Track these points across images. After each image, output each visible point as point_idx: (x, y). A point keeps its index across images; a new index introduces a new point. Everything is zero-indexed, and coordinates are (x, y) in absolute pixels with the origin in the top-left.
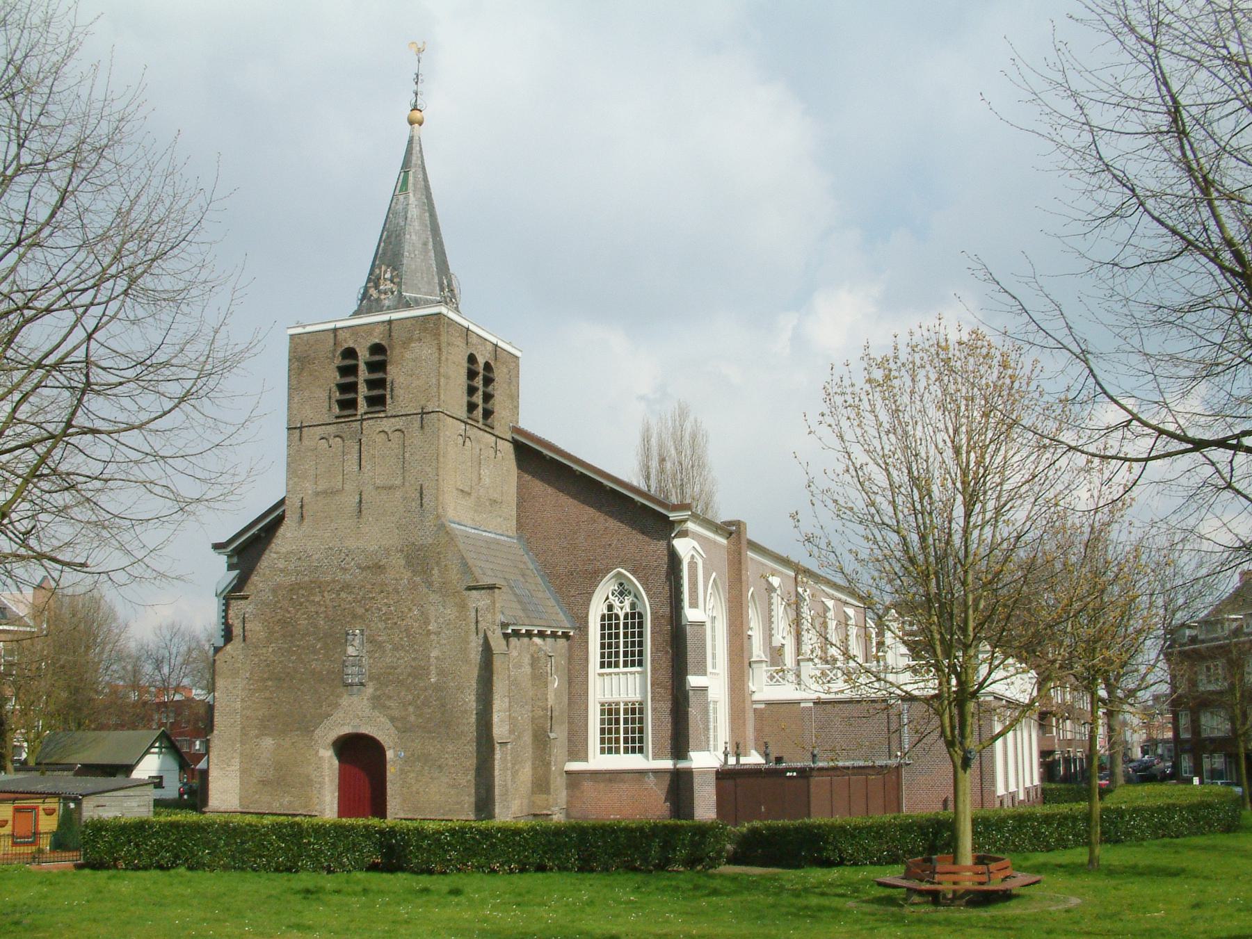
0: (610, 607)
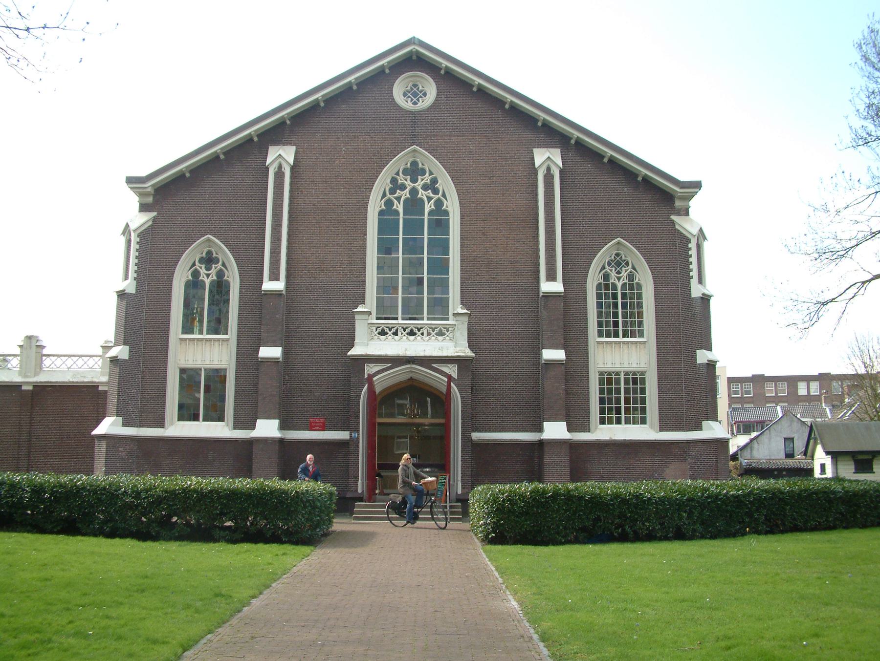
0: (606, 277)
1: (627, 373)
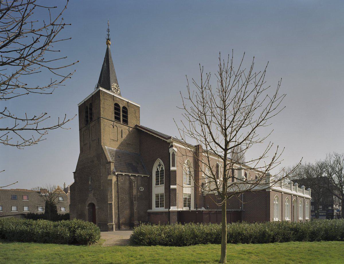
0: (157, 169)
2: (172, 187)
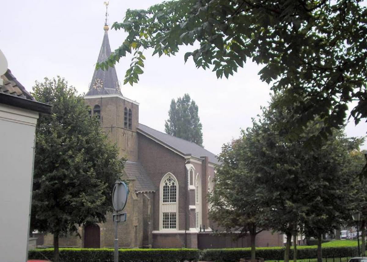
0: (166, 184)
1: (171, 213)
2: (191, 207)
